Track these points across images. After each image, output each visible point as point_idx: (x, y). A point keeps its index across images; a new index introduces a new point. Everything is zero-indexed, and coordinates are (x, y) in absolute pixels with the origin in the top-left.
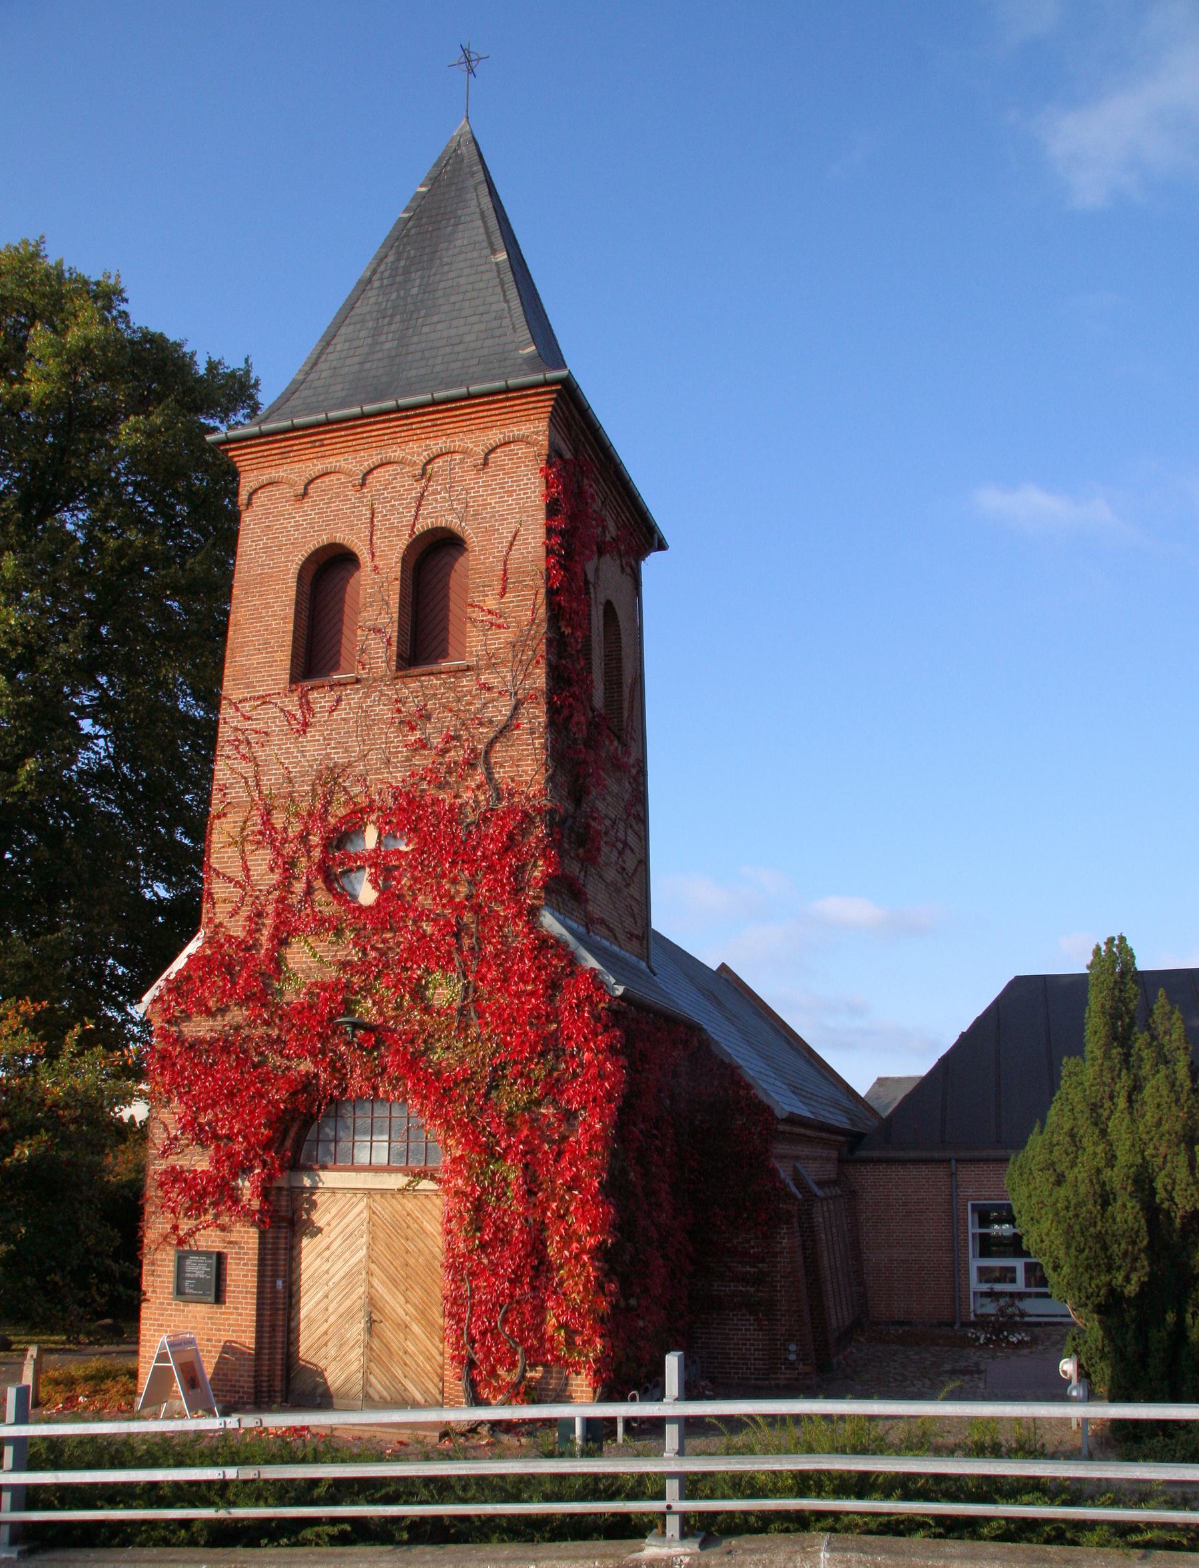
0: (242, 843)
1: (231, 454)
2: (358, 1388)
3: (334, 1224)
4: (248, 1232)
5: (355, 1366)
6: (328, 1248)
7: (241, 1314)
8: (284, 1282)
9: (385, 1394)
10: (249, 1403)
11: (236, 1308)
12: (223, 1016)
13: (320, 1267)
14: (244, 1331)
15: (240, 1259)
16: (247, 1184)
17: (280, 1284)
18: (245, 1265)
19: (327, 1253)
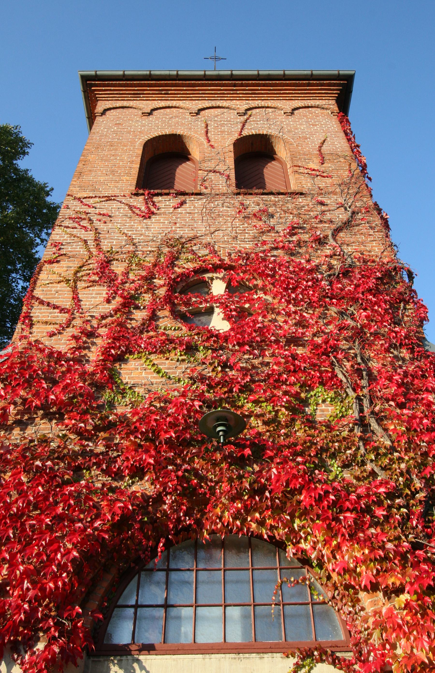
0: (75, 282)
1: (97, 96)
12: (23, 430)
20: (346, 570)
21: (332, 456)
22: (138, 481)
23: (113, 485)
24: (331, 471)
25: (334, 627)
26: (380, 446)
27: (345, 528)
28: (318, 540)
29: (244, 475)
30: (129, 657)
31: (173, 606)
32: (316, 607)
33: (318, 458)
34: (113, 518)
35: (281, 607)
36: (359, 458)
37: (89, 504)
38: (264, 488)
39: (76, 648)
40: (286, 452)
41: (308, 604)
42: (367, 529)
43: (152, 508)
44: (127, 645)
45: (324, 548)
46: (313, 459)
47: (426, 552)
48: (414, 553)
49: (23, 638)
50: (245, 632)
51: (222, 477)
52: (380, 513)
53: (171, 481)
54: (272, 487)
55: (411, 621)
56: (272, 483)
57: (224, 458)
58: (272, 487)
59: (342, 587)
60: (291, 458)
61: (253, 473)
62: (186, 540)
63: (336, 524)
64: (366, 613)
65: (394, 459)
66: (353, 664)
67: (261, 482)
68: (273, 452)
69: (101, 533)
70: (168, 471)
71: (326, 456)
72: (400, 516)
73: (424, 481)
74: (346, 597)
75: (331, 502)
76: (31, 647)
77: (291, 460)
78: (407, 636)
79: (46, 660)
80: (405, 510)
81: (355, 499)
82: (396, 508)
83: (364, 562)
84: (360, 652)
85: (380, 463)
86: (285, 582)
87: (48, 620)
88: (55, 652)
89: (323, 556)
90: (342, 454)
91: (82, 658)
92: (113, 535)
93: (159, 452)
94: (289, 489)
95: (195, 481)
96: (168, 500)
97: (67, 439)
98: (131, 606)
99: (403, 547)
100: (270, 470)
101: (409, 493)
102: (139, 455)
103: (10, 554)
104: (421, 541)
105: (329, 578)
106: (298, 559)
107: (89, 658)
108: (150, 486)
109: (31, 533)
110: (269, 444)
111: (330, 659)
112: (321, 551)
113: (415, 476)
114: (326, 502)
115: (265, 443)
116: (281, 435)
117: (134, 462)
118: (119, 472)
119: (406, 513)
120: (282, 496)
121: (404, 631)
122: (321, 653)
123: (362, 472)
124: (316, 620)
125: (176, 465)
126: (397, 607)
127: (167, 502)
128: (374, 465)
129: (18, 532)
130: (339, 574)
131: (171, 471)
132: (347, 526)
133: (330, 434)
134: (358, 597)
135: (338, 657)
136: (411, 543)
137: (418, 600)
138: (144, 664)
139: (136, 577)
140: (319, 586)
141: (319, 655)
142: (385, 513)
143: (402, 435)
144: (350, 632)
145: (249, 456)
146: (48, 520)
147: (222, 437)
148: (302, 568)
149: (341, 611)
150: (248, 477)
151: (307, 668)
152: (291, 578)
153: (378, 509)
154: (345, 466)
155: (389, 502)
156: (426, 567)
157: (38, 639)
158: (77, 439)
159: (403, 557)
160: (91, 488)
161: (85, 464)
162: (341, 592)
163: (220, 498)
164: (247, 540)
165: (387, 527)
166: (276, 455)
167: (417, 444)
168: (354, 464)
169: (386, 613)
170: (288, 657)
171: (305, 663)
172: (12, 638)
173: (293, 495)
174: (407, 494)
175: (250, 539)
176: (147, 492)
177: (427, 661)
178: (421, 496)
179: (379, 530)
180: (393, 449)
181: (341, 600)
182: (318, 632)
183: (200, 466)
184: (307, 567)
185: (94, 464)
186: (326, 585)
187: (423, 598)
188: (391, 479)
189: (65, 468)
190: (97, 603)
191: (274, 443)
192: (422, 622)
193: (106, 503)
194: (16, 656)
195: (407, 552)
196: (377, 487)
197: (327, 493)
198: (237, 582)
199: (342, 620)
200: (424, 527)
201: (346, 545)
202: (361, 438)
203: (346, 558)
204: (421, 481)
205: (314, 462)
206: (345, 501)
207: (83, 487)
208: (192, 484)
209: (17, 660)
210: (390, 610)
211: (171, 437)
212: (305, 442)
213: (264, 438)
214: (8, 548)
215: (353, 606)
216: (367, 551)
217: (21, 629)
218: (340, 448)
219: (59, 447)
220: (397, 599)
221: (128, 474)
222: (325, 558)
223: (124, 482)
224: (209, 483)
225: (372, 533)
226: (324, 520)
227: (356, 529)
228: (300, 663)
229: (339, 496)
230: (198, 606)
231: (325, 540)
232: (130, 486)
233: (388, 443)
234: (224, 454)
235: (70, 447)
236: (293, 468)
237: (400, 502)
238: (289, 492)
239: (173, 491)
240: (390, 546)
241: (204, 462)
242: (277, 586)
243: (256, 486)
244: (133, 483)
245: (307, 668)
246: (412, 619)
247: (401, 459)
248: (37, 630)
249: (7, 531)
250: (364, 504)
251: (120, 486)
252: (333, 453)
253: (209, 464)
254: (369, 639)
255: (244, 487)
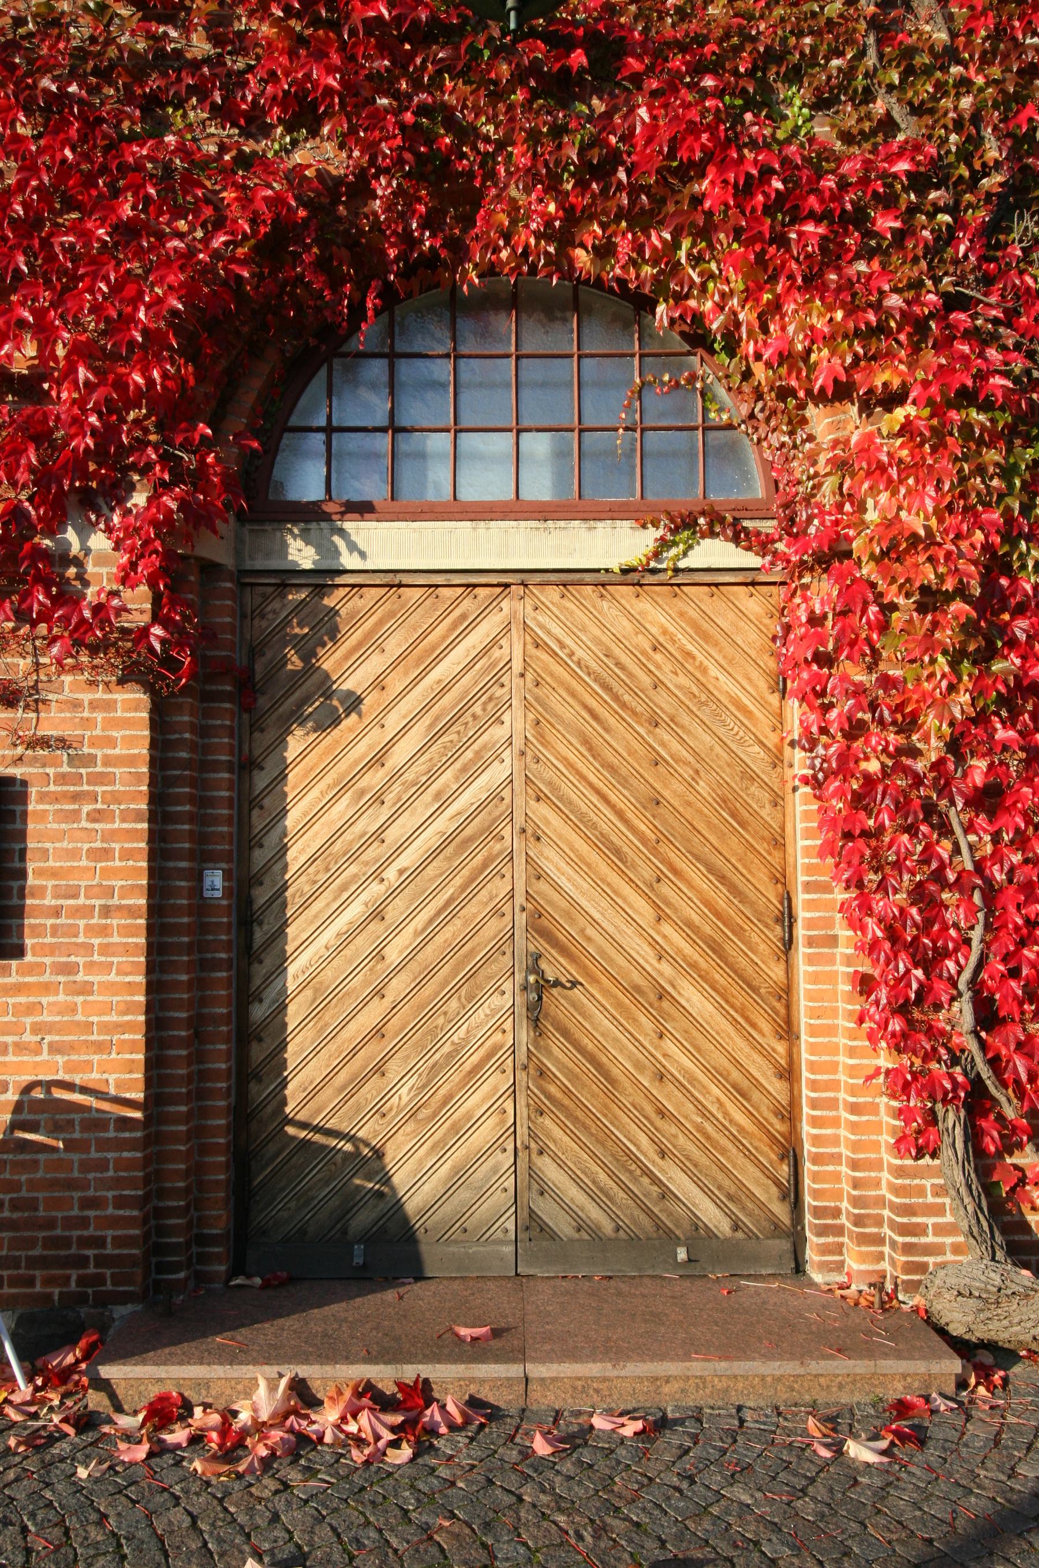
2: (499, 1199)
3: (396, 683)
4: (110, 705)
5: (485, 1133)
6: (378, 760)
7: (85, 989)
8: (227, 876)
9: (595, 1213)
10: (124, 1299)
11: (69, 969)
13: (350, 823)
14: (100, 1047)
15: (76, 797)
16: (99, 542)
17: (215, 880)
18: (96, 816)
19: (375, 779)
20: (785, 357)
21: (791, 75)
22: (306, 140)
23: (247, 149)
24: (785, 118)
25: (746, 476)
26: (920, 45)
27: (797, 260)
28: (731, 291)
29: (567, 124)
30: (323, 524)
31: (404, 430)
32: (712, 435)
33: (756, 80)
34: (255, 233)
35: (638, 435)
36: (860, 82)
37: (195, 196)
38: (614, 159)
39: (212, 503)
40: (677, 62)
41: (696, 428)
42: (850, 262)
43: (347, 208)
44: (316, 504)
45: (743, 307)
46: (741, 83)
47: (974, 317)
48: (946, 318)
49: (101, 483)
50: (560, 480)
51: (513, 130)
52: (887, 223)
53: (386, 139)
54: (634, 158)
55: (909, 459)
56: (633, 146)
57: (519, 78)
58: (634, 158)
59: (773, 394)
60: (688, 80)
61: (590, 119)
62: (429, 289)
63: (778, 250)
64: (817, 444)
65: (947, 82)
66: (773, 541)
67: (608, 144)
68: (642, 62)
69: (233, 266)
70: (377, 110)
71: (777, 73)
72: (932, 232)
73: (1009, 143)
74: (779, 415)
75: (773, 195)
76: (121, 501)
77: (688, 86)
78: (892, 487)
79: (154, 523)
80: (947, 218)
81: (831, 189)
82: (928, 214)
83: (829, 340)
84: (792, 520)
85: (910, 94)
86: (650, 383)
87: (145, 450)
88: (171, 511)
89: (738, 325)
90: (817, 69)
91: (226, 521)
92: (262, 273)
93: (353, 58)
94: (675, 164)
95: (447, 140)
96: (383, 187)
97: (111, 18)
98: (318, 430)
99: (924, 304)
100: (632, 110)
101: (967, 174)
102: (303, 66)
103: (33, 311)
104: (966, 292)
105: (747, 375)
106: (682, 334)
107: (243, 525)
108: (338, 152)
109: (70, 265)
110: (633, 36)
111: (729, 533)
112: (735, 314)
113: (989, 130)
114: (760, 198)
115: (623, 34)
116: (668, 14)
117: (290, 86)
118: (257, 113)
119: (948, 225)
120: (657, 182)
121: (890, 477)
122: (712, 521)
123: (860, 120)
124: (710, 460)
125: (396, 95)
126: (885, 433)
127: (380, 192)
128: (894, 100)
129: (40, 262)
130: (768, 365)
131: (386, 110)
132: (802, 257)
133: (794, 10)
134: (803, 416)
135: (745, 529)
136: (945, 295)
137: (932, 416)
138: (353, 538)
139: (323, 372)
140: (721, 392)
141: (707, 524)
142: (897, 224)
143: (982, 14)
144: (776, 482)
145: (583, 70)
146: (101, 231)
147: (512, 14)
148: (689, 353)
149: (765, 444)
150: (577, 130)
151: (682, 547)
152: (663, 375)
153: (882, 216)
154: (821, 103)
155: (913, 196)
156: (966, 349)
157: (132, 487)
158: (135, 18)
159: (919, 327)
160: (193, 153)
161: (168, 90)
162: (770, 404)
163: (506, 186)
164: (569, 294)
165: (896, 260)
166: (650, 69)
167: (1015, 39)
168: (843, 98)
169: (857, 444)
170: (644, 526)
171: (677, 539)
172: (77, 484)
173: (686, 180)
174: (961, 177)
175: (575, 288)
176: (331, 168)
177: (922, 533)
178: (991, 182)
179: (876, 265)
180: (950, 55)
181: (768, 420)
182: (710, 483)
183: (458, 100)
184: (700, 351)
185: (191, 90)
186: (740, 391)
187: (945, 414)
188: (930, 137)
189: (119, 101)
190: (244, 420)
191: (647, 35)
192: (930, 461)
193: (233, 195)
194: (93, 517)
195: (931, 316)
196: (892, 159)
197: (767, 173)
198: (543, 385)
199: (764, 461)
200: (983, 259)
201: (795, 301)
202: (873, 23)
203: (791, 329)
204: (1003, 143)
205: (744, 91)
206: (809, 193)
207: (173, 152)
208: (439, 149)
209: (98, 523)
210: (869, 437)
211: (381, 16)
212: (727, 36)
213: (623, 20)
214: (25, 297)
215: (791, 433)
216: (839, 315)
217: (92, 467)
218: (814, 49)
219: (93, 40)
220: (887, 416)
221: (279, 118)
222: (744, 329)
223: (273, 141)
224: (481, 146)
225: (859, 273)
226: (747, 244)
227: (822, 263)
228: (669, 537)
229: (795, 183)
230: (462, 431)
231: (747, 290)
232: (288, 152)
233: (942, 36)
234: (518, 65)
235: (123, 40)
236: (690, 104)
237: (939, 198)
238: (675, 172)
239: (394, 165)
240: (894, 301)
241: (468, 89)
242: (632, 392)
243: (595, 156)
244: (294, 143)
245: (682, 547)
246: (912, 455)
247: (964, 84)
248: (127, 469)
249: (11, 258)
250: (851, 202)
251: (264, 151)
252: (794, 66)
253: (483, 92)
254: (814, 496)
255: (564, 159)
